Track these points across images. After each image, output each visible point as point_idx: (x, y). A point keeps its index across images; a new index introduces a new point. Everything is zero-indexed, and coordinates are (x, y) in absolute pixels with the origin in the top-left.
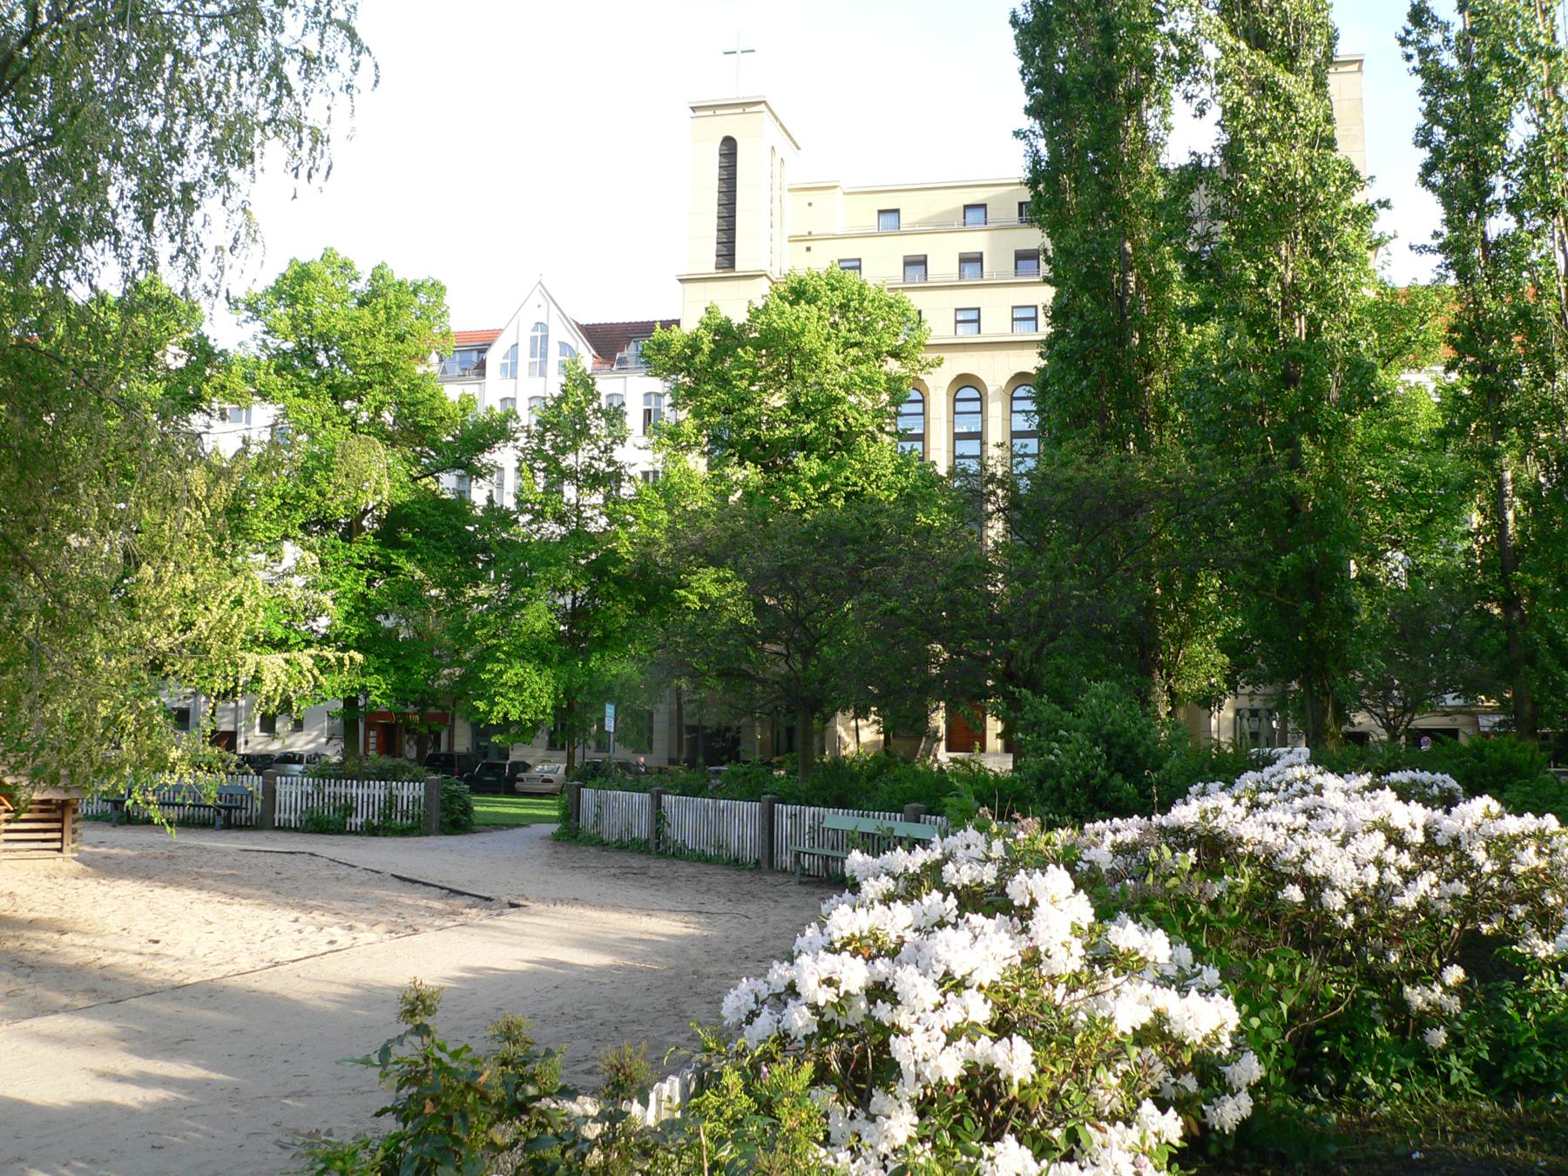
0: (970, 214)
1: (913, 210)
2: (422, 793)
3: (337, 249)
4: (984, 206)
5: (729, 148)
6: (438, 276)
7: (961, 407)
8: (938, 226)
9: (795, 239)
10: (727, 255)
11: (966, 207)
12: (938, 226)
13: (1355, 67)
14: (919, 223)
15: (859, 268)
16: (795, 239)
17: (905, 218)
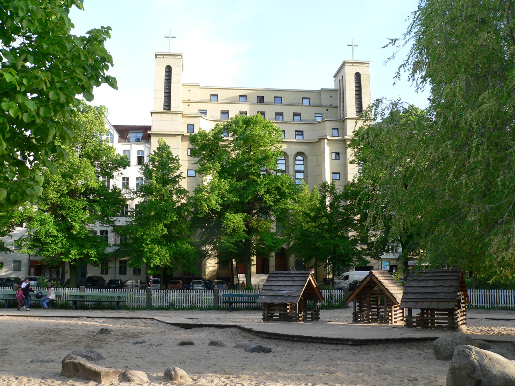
0: (241, 98)
1: (222, 95)
2: (343, 293)
3: (416, 106)
4: (246, 96)
5: (169, 70)
6: (103, 104)
7: (297, 162)
8: (231, 101)
9: (184, 102)
10: (168, 105)
11: (240, 96)
12: (231, 101)
13: (180, 57)
14: (223, 100)
15: (206, 113)
16: (184, 102)
17: (266, 100)
